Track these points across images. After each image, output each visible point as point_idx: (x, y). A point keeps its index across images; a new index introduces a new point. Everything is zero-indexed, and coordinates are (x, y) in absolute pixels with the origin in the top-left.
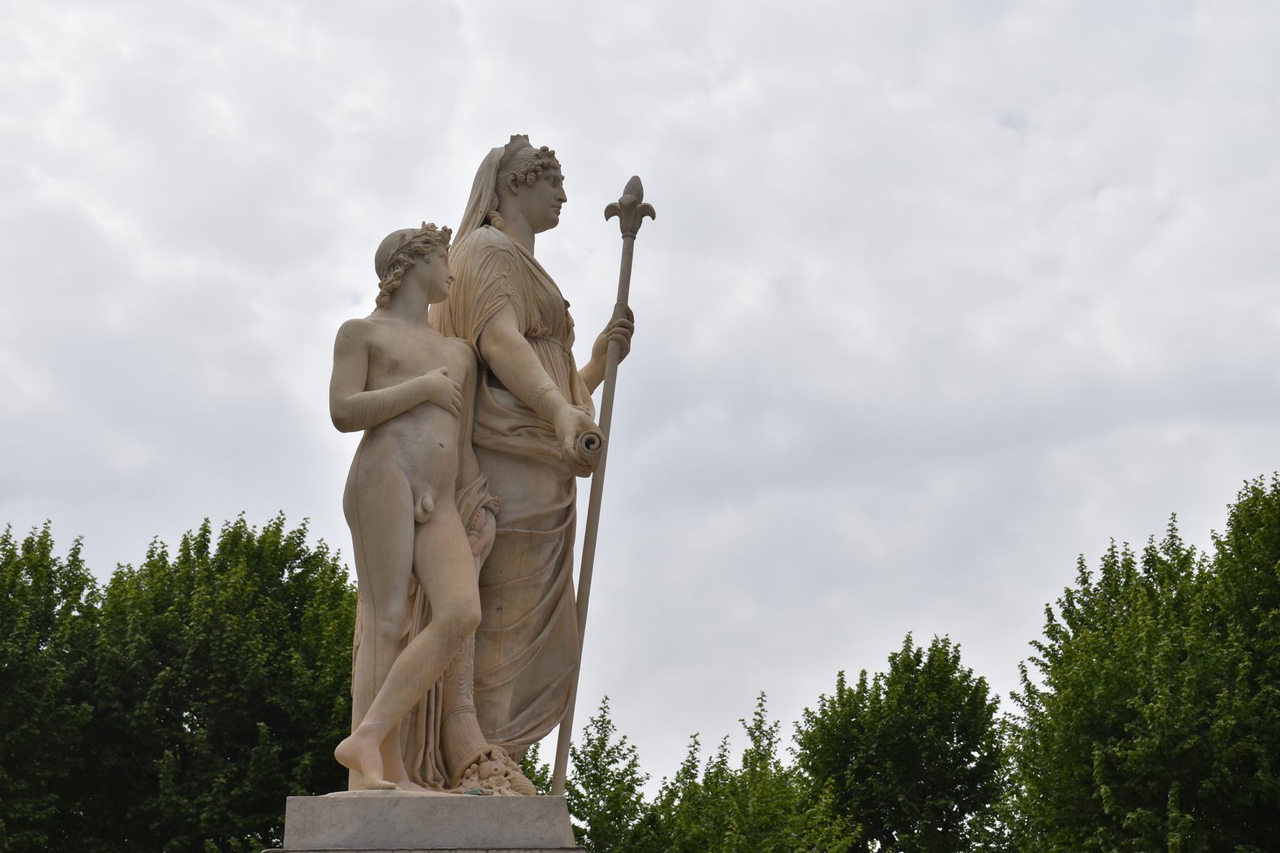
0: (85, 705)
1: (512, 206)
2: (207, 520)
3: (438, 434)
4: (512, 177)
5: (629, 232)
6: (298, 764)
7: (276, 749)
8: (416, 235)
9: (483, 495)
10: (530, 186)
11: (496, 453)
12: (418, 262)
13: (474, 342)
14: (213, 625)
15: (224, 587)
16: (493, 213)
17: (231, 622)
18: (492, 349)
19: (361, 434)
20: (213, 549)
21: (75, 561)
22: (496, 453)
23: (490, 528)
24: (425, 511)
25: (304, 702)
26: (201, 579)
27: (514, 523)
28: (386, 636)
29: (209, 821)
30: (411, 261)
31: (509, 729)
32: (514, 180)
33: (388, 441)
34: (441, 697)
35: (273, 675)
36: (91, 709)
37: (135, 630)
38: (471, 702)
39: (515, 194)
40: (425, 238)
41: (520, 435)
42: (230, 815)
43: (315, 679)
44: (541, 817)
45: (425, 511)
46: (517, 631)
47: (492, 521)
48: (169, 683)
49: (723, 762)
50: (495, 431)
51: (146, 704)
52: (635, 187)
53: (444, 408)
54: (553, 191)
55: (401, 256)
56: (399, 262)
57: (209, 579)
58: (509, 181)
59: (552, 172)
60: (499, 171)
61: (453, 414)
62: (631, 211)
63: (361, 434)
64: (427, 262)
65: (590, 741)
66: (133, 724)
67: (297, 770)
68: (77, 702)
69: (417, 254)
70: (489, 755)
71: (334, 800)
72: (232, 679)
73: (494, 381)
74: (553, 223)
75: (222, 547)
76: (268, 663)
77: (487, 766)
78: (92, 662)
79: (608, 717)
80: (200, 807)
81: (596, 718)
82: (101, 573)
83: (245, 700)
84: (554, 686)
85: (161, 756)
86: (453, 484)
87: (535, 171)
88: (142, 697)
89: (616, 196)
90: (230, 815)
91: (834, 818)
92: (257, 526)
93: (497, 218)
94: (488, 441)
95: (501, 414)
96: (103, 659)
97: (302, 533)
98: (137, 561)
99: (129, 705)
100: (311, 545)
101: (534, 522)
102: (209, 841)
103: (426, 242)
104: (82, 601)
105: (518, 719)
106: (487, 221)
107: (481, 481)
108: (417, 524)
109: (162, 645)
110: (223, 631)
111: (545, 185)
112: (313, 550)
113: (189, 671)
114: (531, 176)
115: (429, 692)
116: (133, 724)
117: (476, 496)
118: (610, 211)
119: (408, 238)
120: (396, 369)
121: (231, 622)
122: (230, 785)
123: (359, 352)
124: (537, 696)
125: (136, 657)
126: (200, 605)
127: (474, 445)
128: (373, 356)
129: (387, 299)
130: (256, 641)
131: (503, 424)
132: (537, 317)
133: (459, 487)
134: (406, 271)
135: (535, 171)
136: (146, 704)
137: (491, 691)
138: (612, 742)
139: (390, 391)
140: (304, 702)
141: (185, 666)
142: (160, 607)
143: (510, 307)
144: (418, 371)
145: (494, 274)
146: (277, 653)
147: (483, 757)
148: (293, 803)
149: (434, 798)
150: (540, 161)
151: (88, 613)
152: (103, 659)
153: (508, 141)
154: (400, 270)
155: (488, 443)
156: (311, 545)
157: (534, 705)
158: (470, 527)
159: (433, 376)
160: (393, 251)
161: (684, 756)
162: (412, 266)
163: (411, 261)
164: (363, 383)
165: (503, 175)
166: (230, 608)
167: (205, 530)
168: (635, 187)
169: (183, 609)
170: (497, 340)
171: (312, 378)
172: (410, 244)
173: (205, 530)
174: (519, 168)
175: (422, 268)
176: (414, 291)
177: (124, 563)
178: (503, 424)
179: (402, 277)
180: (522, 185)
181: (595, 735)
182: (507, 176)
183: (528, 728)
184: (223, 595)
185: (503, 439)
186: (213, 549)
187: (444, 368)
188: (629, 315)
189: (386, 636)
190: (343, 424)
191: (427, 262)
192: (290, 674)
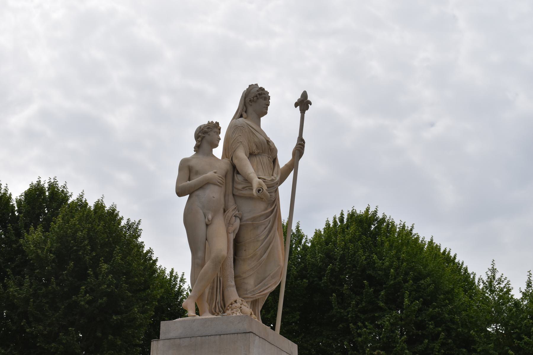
0: (305, 280)
1: (250, 110)
2: (342, 211)
3: (214, 194)
6: (380, 295)
7: (372, 290)
8: (205, 126)
9: (234, 212)
10: (255, 102)
11: (240, 197)
12: (206, 136)
13: (230, 159)
14: (345, 248)
15: (348, 234)
17: (351, 246)
18: (235, 161)
20: (345, 220)
21: (298, 230)
22: (240, 197)
23: (237, 223)
24: (209, 220)
25: (380, 272)
26: (340, 232)
27: (247, 220)
29: (352, 317)
30: (203, 135)
31: (253, 291)
32: (250, 101)
35: (368, 263)
36: (307, 281)
37: (319, 253)
38: (233, 283)
39: (251, 105)
42: (359, 314)
43: (383, 264)
44: (240, 322)
45: (209, 220)
46: (252, 257)
47: (238, 220)
48: (332, 270)
50: (238, 189)
51: (325, 278)
52: (305, 95)
53: (215, 184)
54: (264, 102)
56: (200, 136)
57: (343, 231)
58: (248, 101)
59: (263, 95)
61: (219, 186)
62: (303, 104)
64: (209, 135)
65: (489, 277)
66: (322, 285)
67: (380, 297)
68: (302, 279)
69: (205, 133)
70: (236, 302)
72: (354, 266)
73: (238, 173)
74: (266, 113)
75: (348, 219)
76: (365, 260)
78: (305, 266)
79: (495, 267)
80: (348, 312)
81: (490, 268)
82: (309, 234)
83: (359, 273)
84: (271, 274)
85: (332, 296)
86: (222, 211)
87: (256, 96)
88: (324, 276)
90: (359, 314)
92: (360, 210)
93: (244, 115)
95: (239, 184)
96: (309, 263)
97: (376, 211)
98: (321, 227)
99: (320, 279)
100: (380, 215)
101: (254, 219)
102: (351, 324)
103: (209, 128)
104: (303, 243)
105: (257, 287)
106: (241, 116)
107: (234, 207)
108: (207, 225)
109: (329, 257)
110: (349, 250)
111: (262, 101)
112: (381, 217)
113: (339, 265)
114: (255, 98)
115: (213, 282)
116: (322, 285)
117: (231, 212)
120: (197, 173)
121: (351, 246)
122: (357, 304)
123: (187, 169)
124: (265, 279)
125: (320, 262)
126: (340, 241)
127: (234, 195)
130: (361, 251)
131: (240, 187)
132: (254, 148)
133: (225, 211)
134: (202, 139)
135: (256, 96)
136: (325, 278)
137: (244, 279)
138: (497, 276)
139: (196, 180)
140: (380, 272)
141: (337, 263)
142: (327, 244)
143: (241, 146)
145: (236, 135)
146: (369, 256)
147: (233, 302)
148: (163, 323)
149: (211, 318)
151: (305, 247)
152: (309, 263)
153: (248, 87)
156: (380, 215)
157: (263, 282)
158: (228, 224)
159: (210, 174)
161: (526, 279)
162: (204, 137)
163: (203, 135)
164: (188, 178)
165: (247, 99)
166: (351, 241)
167: (342, 214)
168: (305, 95)
169: (335, 244)
171: (171, 179)
172: (203, 129)
173: (342, 214)
174: (252, 96)
175: (207, 137)
177: (317, 229)
178: (240, 187)
179: (202, 139)
180: (255, 101)
181: (490, 273)
182: (248, 100)
183: (262, 290)
184: (347, 237)
185: (241, 192)
186: (345, 220)
187: (216, 171)
188: (303, 141)
190: (180, 193)
191: (209, 135)
192: (374, 263)
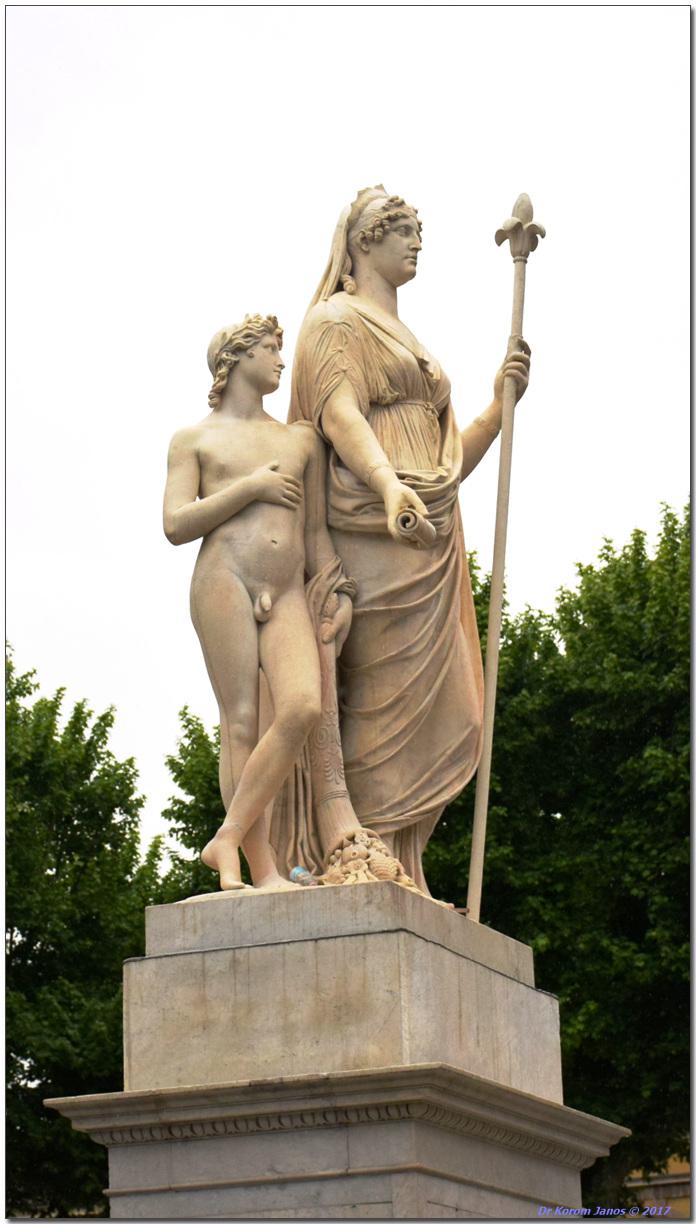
1: (365, 265)
4: (361, 235)
5: (521, 256)
12: (243, 358)
16: (347, 277)
18: (331, 430)
19: (201, 540)
24: (263, 609)
27: (373, 601)
28: (239, 738)
30: (234, 358)
32: (364, 239)
33: (217, 546)
34: (309, 783)
38: (342, 787)
39: (367, 253)
40: (245, 332)
41: (366, 513)
45: (263, 609)
49: (182, 862)
50: (343, 512)
53: (274, 503)
55: (224, 355)
58: (358, 240)
60: (348, 232)
63: (201, 540)
64: (251, 356)
69: (239, 350)
70: (352, 839)
71: (186, 905)
77: (350, 850)
89: (505, 218)
91: (77, 903)
93: (349, 282)
94: (340, 522)
95: (344, 495)
106: (340, 287)
108: (260, 624)
118: (500, 237)
119: (229, 335)
120: (224, 473)
127: (330, 528)
128: (202, 463)
129: (216, 400)
133: (307, 578)
139: (221, 493)
143: (346, 383)
144: (244, 470)
145: (330, 351)
147: (346, 841)
150: (386, 214)
154: (224, 370)
155: (340, 524)
160: (217, 351)
162: (236, 363)
165: (353, 234)
168: (525, 210)
170: (334, 419)
172: (231, 341)
174: (367, 223)
176: (241, 388)
178: (348, 504)
182: (356, 235)
185: (351, 519)
187: (275, 463)
189: (239, 738)
190: (177, 538)
